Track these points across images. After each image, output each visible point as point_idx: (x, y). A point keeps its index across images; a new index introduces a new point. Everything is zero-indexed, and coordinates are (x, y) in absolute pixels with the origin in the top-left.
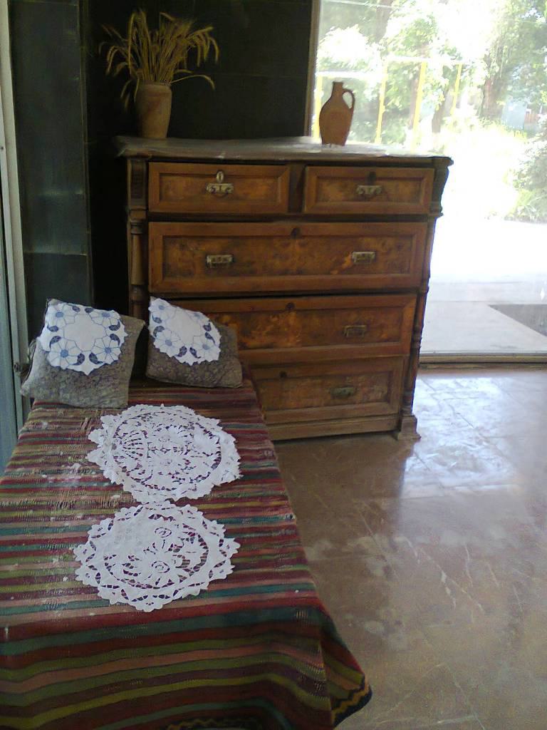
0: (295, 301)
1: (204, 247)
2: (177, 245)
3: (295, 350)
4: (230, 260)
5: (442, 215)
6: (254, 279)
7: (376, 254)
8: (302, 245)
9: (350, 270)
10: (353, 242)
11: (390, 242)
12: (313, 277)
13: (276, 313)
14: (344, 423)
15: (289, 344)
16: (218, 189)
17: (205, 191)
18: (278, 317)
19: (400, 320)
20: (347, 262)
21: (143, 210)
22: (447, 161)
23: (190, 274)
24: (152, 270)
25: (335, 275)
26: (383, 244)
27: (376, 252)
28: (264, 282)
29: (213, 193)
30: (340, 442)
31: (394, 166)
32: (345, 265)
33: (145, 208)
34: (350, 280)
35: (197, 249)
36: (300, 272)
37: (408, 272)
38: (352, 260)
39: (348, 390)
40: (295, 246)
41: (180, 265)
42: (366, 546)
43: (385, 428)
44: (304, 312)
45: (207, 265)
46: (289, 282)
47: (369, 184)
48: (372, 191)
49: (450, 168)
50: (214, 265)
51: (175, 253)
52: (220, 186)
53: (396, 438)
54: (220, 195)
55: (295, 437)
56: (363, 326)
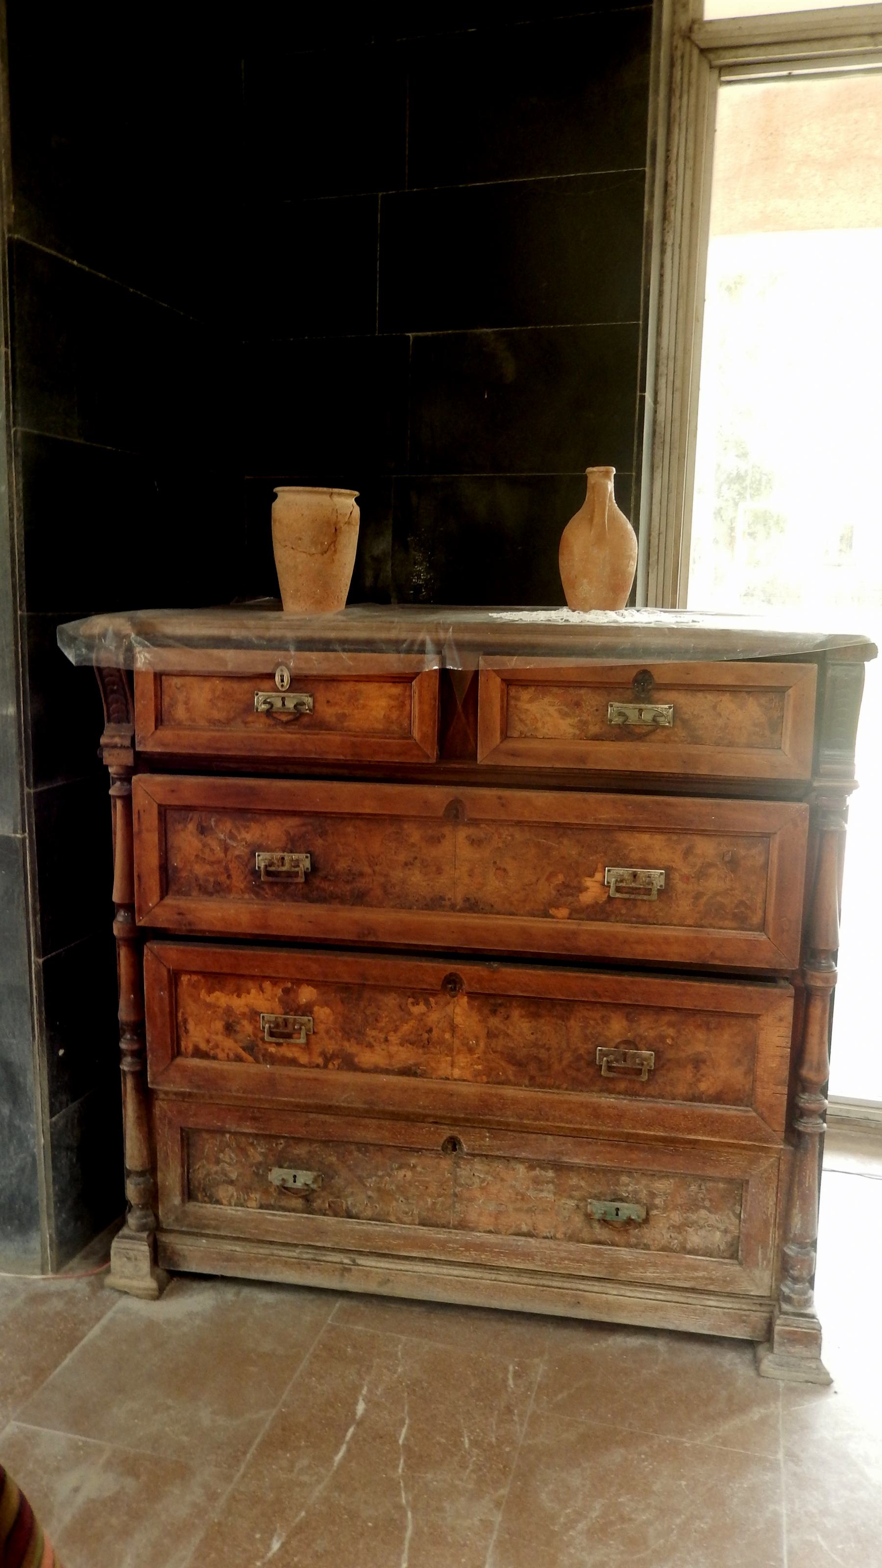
0: (467, 970)
1: (252, 834)
2: (191, 827)
3: (464, 1089)
4: (306, 864)
5: (856, 787)
6: (359, 914)
7: (667, 877)
8: (475, 842)
9: (601, 911)
10: (603, 839)
11: (706, 848)
12: (502, 921)
13: (422, 994)
14: (612, 1293)
15: (457, 1073)
16: (278, 704)
17: (249, 708)
18: (427, 1003)
19: (751, 1051)
20: (592, 891)
21: (122, 747)
22: (863, 650)
23: (218, 890)
24: (139, 876)
25: (561, 921)
26: (688, 852)
27: (669, 871)
28: (382, 919)
29: (269, 713)
30: (618, 1341)
31: (288, 811)
32: (586, 898)
33: (127, 743)
34: (593, 934)
35: (232, 837)
36: (472, 906)
37: (762, 927)
38: (605, 886)
39: (629, 1210)
40: (458, 843)
41: (200, 870)
42: (186, 1253)
43: (740, 1333)
44: (490, 1001)
45: (255, 873)
46: (444, 927)
47: (637, 699)
48: (647, 717)
49: (870, 667)
50: (268, 873)
51: (186, 839)
52: (283, 699)
53: (756, 1362)
54: (284, 718)
55: (495, 1304)
56: (645, 1053)
